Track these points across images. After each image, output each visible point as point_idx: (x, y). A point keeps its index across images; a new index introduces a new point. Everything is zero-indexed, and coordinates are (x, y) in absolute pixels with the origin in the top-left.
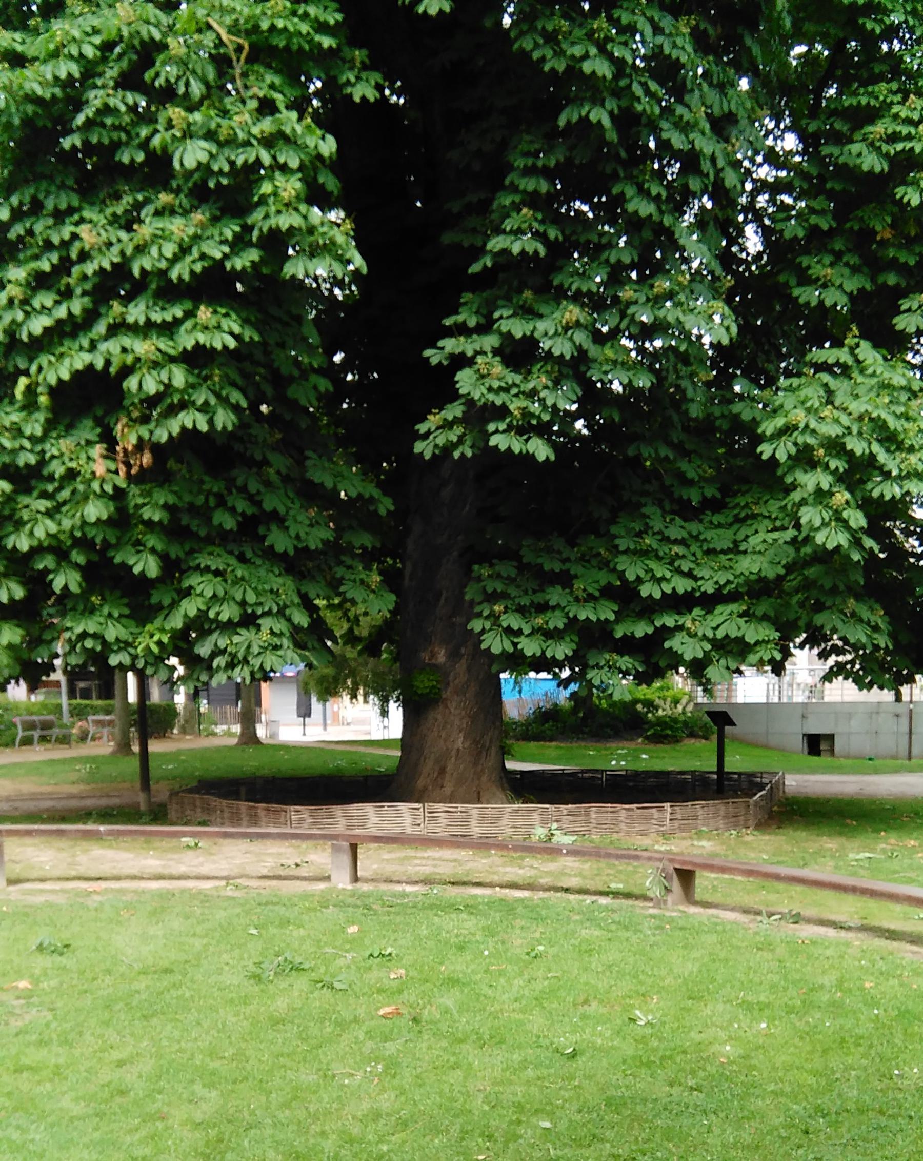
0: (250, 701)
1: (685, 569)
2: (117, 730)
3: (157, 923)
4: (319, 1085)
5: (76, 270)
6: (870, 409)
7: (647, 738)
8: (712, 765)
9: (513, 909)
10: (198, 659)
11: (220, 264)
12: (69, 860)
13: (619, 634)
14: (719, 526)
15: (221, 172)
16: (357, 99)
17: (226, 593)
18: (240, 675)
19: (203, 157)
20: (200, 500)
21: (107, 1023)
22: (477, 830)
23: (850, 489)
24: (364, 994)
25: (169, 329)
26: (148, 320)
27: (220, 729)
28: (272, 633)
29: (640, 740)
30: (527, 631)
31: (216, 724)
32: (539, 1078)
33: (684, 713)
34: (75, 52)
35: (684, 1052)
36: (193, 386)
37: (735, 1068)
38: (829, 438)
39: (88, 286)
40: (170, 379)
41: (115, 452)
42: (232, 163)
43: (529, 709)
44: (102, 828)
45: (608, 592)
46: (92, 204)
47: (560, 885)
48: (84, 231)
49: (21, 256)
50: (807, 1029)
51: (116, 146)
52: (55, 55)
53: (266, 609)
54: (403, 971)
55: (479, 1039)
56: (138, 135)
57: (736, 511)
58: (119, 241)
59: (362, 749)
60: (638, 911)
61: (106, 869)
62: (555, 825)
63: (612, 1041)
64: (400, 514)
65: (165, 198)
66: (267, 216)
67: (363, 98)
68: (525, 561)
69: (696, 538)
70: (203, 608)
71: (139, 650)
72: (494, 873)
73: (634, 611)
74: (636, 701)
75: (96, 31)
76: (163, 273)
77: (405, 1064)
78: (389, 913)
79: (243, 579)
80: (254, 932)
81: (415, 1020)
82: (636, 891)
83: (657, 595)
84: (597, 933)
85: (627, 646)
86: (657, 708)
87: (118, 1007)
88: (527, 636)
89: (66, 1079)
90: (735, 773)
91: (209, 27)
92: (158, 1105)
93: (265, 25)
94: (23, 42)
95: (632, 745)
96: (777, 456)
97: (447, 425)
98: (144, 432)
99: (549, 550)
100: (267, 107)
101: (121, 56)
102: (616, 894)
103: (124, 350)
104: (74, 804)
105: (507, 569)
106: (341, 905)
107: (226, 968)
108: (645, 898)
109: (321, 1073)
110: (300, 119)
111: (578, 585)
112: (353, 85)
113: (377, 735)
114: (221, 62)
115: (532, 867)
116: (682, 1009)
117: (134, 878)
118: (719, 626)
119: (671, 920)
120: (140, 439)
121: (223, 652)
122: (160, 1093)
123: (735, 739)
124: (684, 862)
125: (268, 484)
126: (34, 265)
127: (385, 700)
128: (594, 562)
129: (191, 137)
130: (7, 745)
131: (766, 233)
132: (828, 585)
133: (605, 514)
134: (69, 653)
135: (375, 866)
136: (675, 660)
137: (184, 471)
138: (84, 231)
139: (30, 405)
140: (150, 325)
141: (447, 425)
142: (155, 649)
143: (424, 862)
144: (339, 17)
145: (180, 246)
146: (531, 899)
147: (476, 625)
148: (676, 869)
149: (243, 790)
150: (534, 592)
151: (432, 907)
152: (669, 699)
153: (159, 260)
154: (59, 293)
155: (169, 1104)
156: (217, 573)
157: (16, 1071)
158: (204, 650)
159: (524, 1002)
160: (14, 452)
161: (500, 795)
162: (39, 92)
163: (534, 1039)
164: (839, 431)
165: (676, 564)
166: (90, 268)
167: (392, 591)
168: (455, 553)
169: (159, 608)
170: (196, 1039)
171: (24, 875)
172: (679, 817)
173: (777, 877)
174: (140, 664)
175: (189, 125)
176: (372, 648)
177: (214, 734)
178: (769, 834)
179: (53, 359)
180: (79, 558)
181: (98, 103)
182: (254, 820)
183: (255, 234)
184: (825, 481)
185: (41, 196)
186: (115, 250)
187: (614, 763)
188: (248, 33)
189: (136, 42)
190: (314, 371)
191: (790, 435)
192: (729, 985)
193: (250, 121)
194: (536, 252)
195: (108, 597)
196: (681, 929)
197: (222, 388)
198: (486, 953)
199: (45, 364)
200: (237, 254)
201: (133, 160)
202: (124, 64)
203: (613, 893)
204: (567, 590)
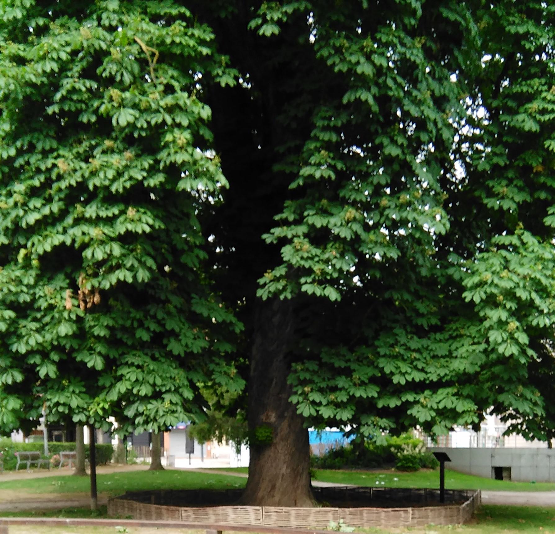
2: (77, 461)
5: (55, 186)
6: (530, 273)
11: (141, 183)
15: (142, 128)
16: (223, 85)
18: (151, 428)
19: (131, 119)
20: (128, 323)
23: (519, 320)
25: (110, 221)
26: (98, 216)
27: (139, 460)
28: (171, 403)
29: (393, 469)
30: (324, 403)
34: (55, 57)
39: (62, 195)
40: (111, 251)
41: (77, 294)
42: (149, 123)
43: (326, 450)
44: (68, 520)
45: (373, 380)
46: (65, 146)
48: (60, 162)
49: (22, 177)
51: (79, 112)
52: (43, 58)
53: (168, 388)
56: (92, 105)
57: (450, 333)
58: (81, 168)
59: (225, 473)
64: (249, 333)
65: (108, 143)
67: (227, 84)
68: (324, 360)
70: (130, 388)
71: (91, 413)
74: (390, 446)
76: (107, 188)
79: (153, 370)
85: (385, 412)
88: (325, 406)
91: (135, 42)
93: (168, 41)
95: (388, 472)
97: (276, 279)
98: (95, 282)
100: (169, 90)
103: (84, 234)
104: (50, 505)
105: (313, 366)
111: (356, 376)
112: (221, 77)
113: (234, 464)
114: (143, 62)
120: (93, 287)
121: (142, 414)
126: (30, 182)
127: (239, 443)
128: (365, 362)
129: (124, 107)
130: (10, 469)
131: (467, 166)
134: (49, 414)
136: (414, 422)
137: (119, 306)
138: (60, 162)
139: (27, 266)
141: (276, 279)
142: (101, 413)
144: (213, 36)
147: (294, 399)
149: (153, 498)
150: (329, 379)
153: (104, 180)
154: (45, 199)
156: (138, 367)
160: (17, 294)
161: (308, 502)
162: (34, 80)
164: (512, 285)
166: (63, 185)
167: (243, 378)
169: (103, 388)
174: (92, 421)
175: (123, 100)
176: (231, 412)
177: (135, 463)
179: (41, 238)
180: (55, 357)
181: (69, 87)
182: (160, 516)
183: (162, 165)
184: (504, 315)
185: (34, 142)
186: (79, 174)
188: (158, 45)
189: (92, 51)
193: (159, 98)
195: (73, 381)
197: (142, 257)
199: (36, 241)
201: (89, 121)
202: (84, 63)
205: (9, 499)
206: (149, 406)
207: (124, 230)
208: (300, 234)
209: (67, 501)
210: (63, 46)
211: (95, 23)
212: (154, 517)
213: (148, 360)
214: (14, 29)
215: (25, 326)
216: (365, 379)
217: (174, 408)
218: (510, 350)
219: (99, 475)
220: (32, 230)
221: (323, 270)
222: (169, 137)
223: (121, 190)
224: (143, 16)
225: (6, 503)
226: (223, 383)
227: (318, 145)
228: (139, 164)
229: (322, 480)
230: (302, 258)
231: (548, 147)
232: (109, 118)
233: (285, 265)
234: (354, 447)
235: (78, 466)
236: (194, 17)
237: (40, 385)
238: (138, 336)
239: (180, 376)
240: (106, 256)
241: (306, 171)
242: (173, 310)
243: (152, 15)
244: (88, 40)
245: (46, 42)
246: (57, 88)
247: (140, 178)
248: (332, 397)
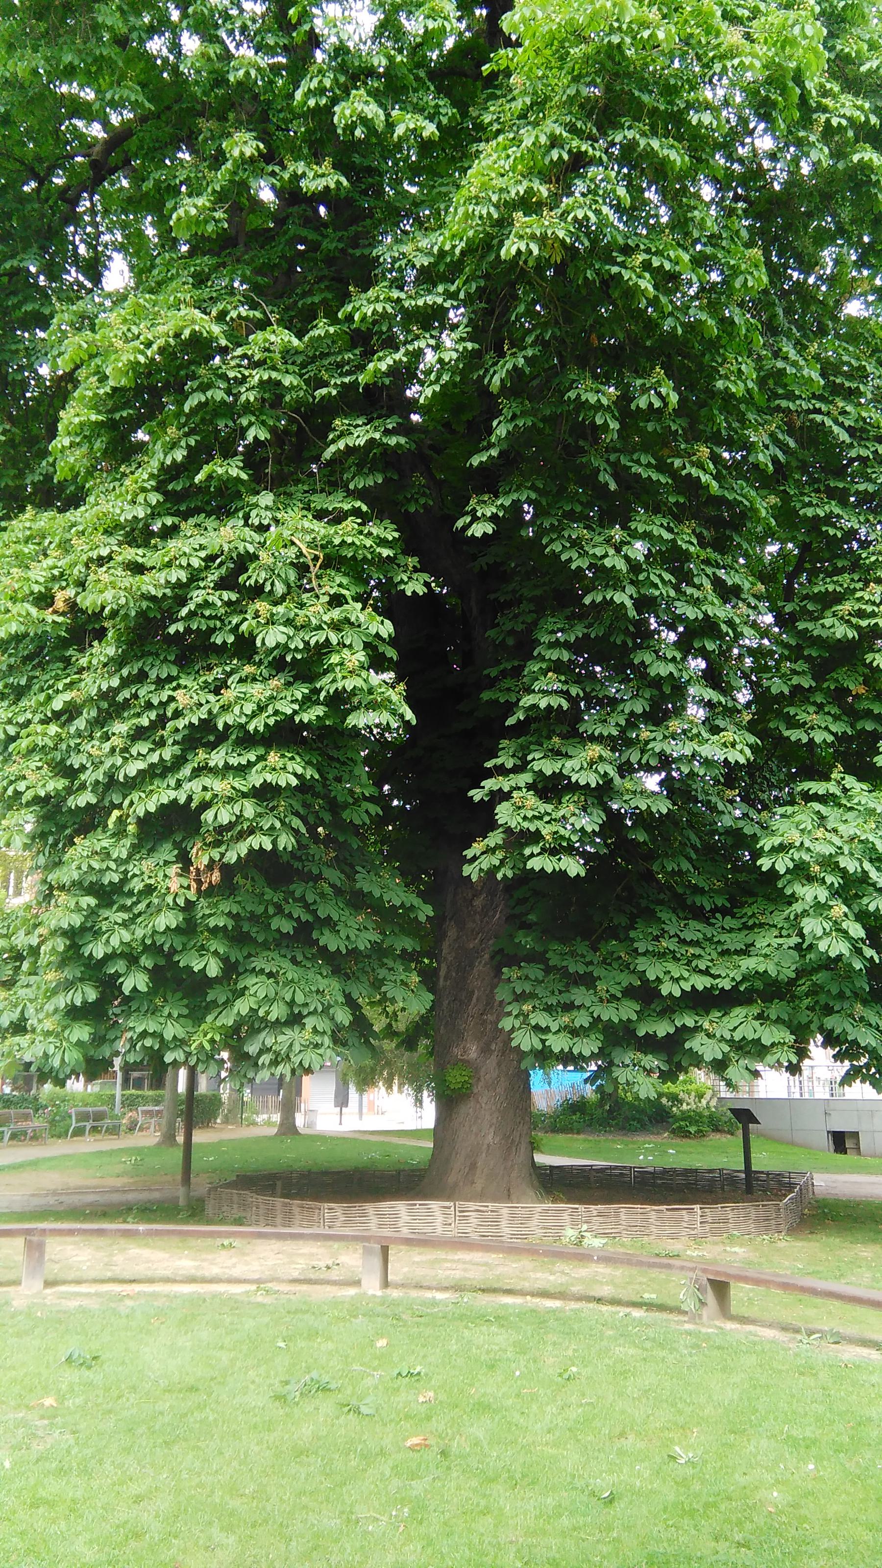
0: (291, 1092)
1: (703, 968)
2: (164, 1121)
3: (186, 1333)
4: (341, 1532)
5: (170, 725)
6: (859, 833)
7: (673, 1132)
8: (738, 1164)
9: (545, 1321)
10: (247, 1056)
11: (291, 717)
12: (106, 1259)
13: (641, 1033)
14: (731, 930)
15: (296, 650)
16: (409, 593)
17: (276, 994)
18: (283, 1069)
19: (282, 639)
20: (260, 910)
21: (127, 1450)
22: (508, 1230)
23: (846, 902)
24: (391, 1421)
25: (242, 770)
27: (261, 1118)
28: (315, 1030)
30: (554, 1027)
31: (257, 1114)
32: (575, 1529)
34: (184, 564)
35: (729, 1499)
36: (260, 815)
37: (784, 1519)
38: (824, 856)
39: (178, 737)
40: (241, 811)
41: (189, 872)
42: (307, 643)
43: (557, 1100)
44: (141, 1227)
45: (629, 992)
47: (592, 1293)
48: (179, 694)
49: (126, 714)
50: (858, 1472)
51: (212, 631)
52: (169, 565)
53: (312, 1009)
54: (431, 1394)
55: (511, 1478)
56: (230, 622)
57: (744, 920)
58: (208, 702)
59: (395, 1140)
60: (673, 1326)
61: (141, 1270)
62: (585, 1227)
63: (651, 1483)
64: (437, 921)
65: (248, 669)
66: (334, 681)
67: (414, 592)
68: (551, 963)
69: (710, 940)
70: (255, 1007)
71: (193, 1048)
72: (525, 1279)
73: (655, 1011)
74: (660, 1095)
75: (202, 547)
76: (242, 727)
77: (432, 1508)
78: (418, 1324)
79: (292, 981)
80: (282, 1345)
81: (443, 1453)
82: (670, 1303)
83: (677, 993)
84: (632, 1351)
86: (681, 1102)
87: (140, 1431)
88: (556, 1033)
89: (81, 1516)
90: (762, 1172)
91: (293, 543)
92: (173, 1551)
93: (337, 541)
94: (144, 556)
95: (658, 1139)
96: (777, 867)
98: (215, 854)
99: (573, 954)
100: (337, 601)
101: (222, 564)
102: (650, 1306)
103: (205, 789)
104: (116, 1198)
105: (535, 971)
106: (370, 1314)
107: (252, 1387)
108: (678, 1310)
109: (344, 1516)
110: (363, 609)
111: (601, 986)
112: (406, 583)
113: (411, 1125)
114: (302, 569)
115: (563, 1272)
116: (723, 1445)
117: (167, 1280)
118: (735, 1028)
119: (708, 1338)
120: (212, 861)
121: (269, 1050)
122: (176, 1537)
123: (760, 1135)
124: (718, 1273)
125: (322, 895)
126: (135, 721)
127: (419, 1090)
128: (615, 965)
129: (273, 624)
130: (59, 1137)
132: (835, 991)
133: (624, 921)
134: (129, 1051)
135: (406, 1270)
136: (697, 1060)
137: (248, 886)
138: (179, 694)
139: (120, 833)
140: (227, 767)
142: (207, 1046)
144: (396, 535)
145: (258, 706)
146: (561, 1310)
147: (506, 1024)
150: (560, 992)
151: (461, 1317)
152: (693, 1094)
153: (240, 717)
154: (154, 741)
155: (185, 1551)
156: (270, 975)
157: (32, 1506)
158: (252, 1049)
159: (557, 1434)
160: (101, 871)
161: (531, 1193)
162: (153, 592)
163: (569, 1479)
164: (833, 850)
165: (694, 964)
166: (181, 723)
167: (430, 990)
168: (487, 956)
170: (216, 1472)
171: (62, 1276)
172: (709, 1219)
173: (814, 1292)
174: (193, 1061)
175: (272, 615)
176: (409, 1042)
177: (254, 1124)
178: (802, 1240)
179: (143, 795)
180: (147, 962)
181: (200, 600)
182: (288, 1221)
183: (323, 694)
184: (823, 895)
185: (147, 669)
186: (204, 709)
187: (641, 1157)
188: (323, 547)
189: (234, 555)
190: (366, 799)
191: (787, 853)
192: (771, 1417)
193: (321, 611)
194: (560, 706)
195: (169, 999)
196: (719, 1348)
197: (285, 816)
198: (518, 1373)
199: (136, 800)
200: (305, 711)
201: (225, 642)
202: (223, 570)
203: (646, 1304)
204: (592, 991)
205: (53, 1187)
206: (281, 1038)
207: (262, 781)
208: (523, 785)
210: (196, 550)
211: (242, 522)
213: (286, 964)
214: (133, 530)
215: (106, 919)
216: (616, 991)
217: (318, 1039)
218: (839, 948)
219: (200, 1145)
221: (556, 833)
222: (335, 659)
223: (261, 729)
224: (305, 512)
225: (47, 1195)
226: (399, 998)
227: (544, 666)
228: (289, 694)
229: (552, 1153)
230: (525, 818)
231: (872, 662)
232: (252, 638)
233: (501, 830)
234: (602, 1098)
235: (165, 1129)
236: (372, 512)
237: (120, 1005)
238: (274, 927)
239: (333, 987)
240: (234, 819)
241: (527, 700)
242: (328, 890)
243: (316, 511)
244: (230, 542)
245: (174, 545)
246: (183, 601)
247: (289, 712)
248: (566, 1019)
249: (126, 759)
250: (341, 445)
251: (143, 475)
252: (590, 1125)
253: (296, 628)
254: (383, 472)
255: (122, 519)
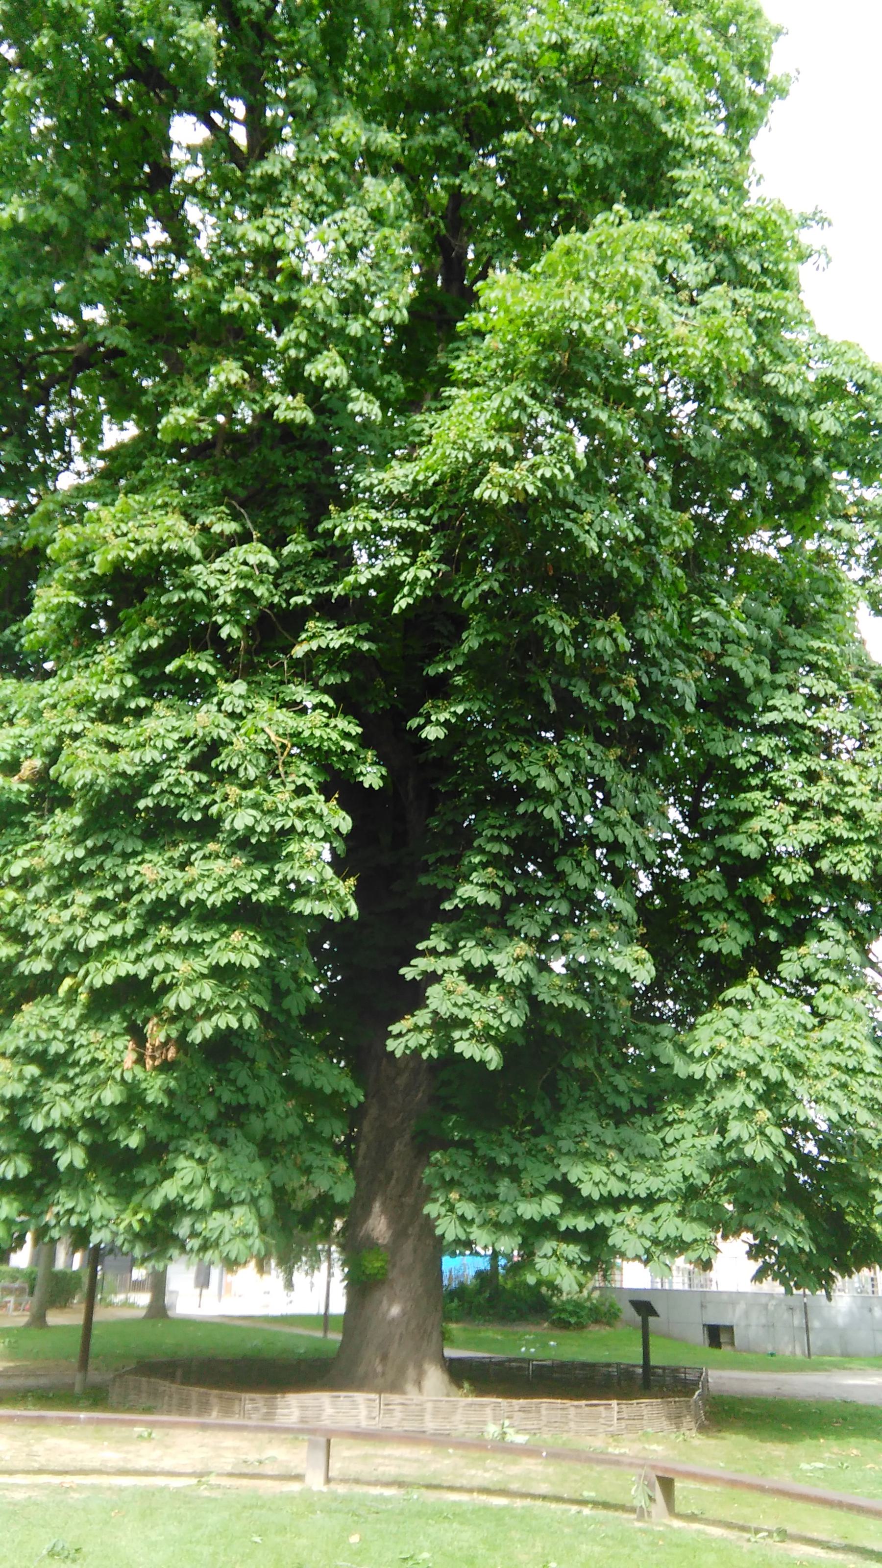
5: (135, 899)
7: (553, 1323)
15: (262, 833)
16: (366, 785)
19: (250, 822)
26: (190, 939)
29: (546, 1325)
33: (589, 1298)
46: (153, 849)
48: (143, 869)
49: (88, 885)
51: (179, 808)
52: (140, 745)
59: (276, 1328)
75: (174, 729)
80: (257, 1539)
85: (571, 1236)
91: (263, 730)
97: (417, 1029)
100: (302, 791)
102: (595, 1504)
105: (463, 1158)
124: (666, 1470)
128: (540, 1157)
131: (655, 878)
141: (417, 1029)
143: (387, 1462)
144: (360, 730)
148: (659, 1478)
149: (179, 1373)
151: (419, 1514)
154: (116, 914)
160: (48, 1042)
169: (142, 1184)
172: (625, 1416)
179: (99, 965)
180: (82, 1136)
181: (171, 779)
188: (292, 735)
189: (208, 739)
196: (678, 1546)
199: (92, 970)
201: (191, 819)
209: (27, 1376)
211: (215, 708)
212: (195, 1407)
214: (104, 708)
220: (88, 955)
232: (220, 818)
245: (149, 724)
247: (248, 890)
249: (86, 929)
250: (314, 645)
251: (291, 723)
252: (469, 1313)
253: (262, 811)
254: (350, 671)
255: (97, 697)
